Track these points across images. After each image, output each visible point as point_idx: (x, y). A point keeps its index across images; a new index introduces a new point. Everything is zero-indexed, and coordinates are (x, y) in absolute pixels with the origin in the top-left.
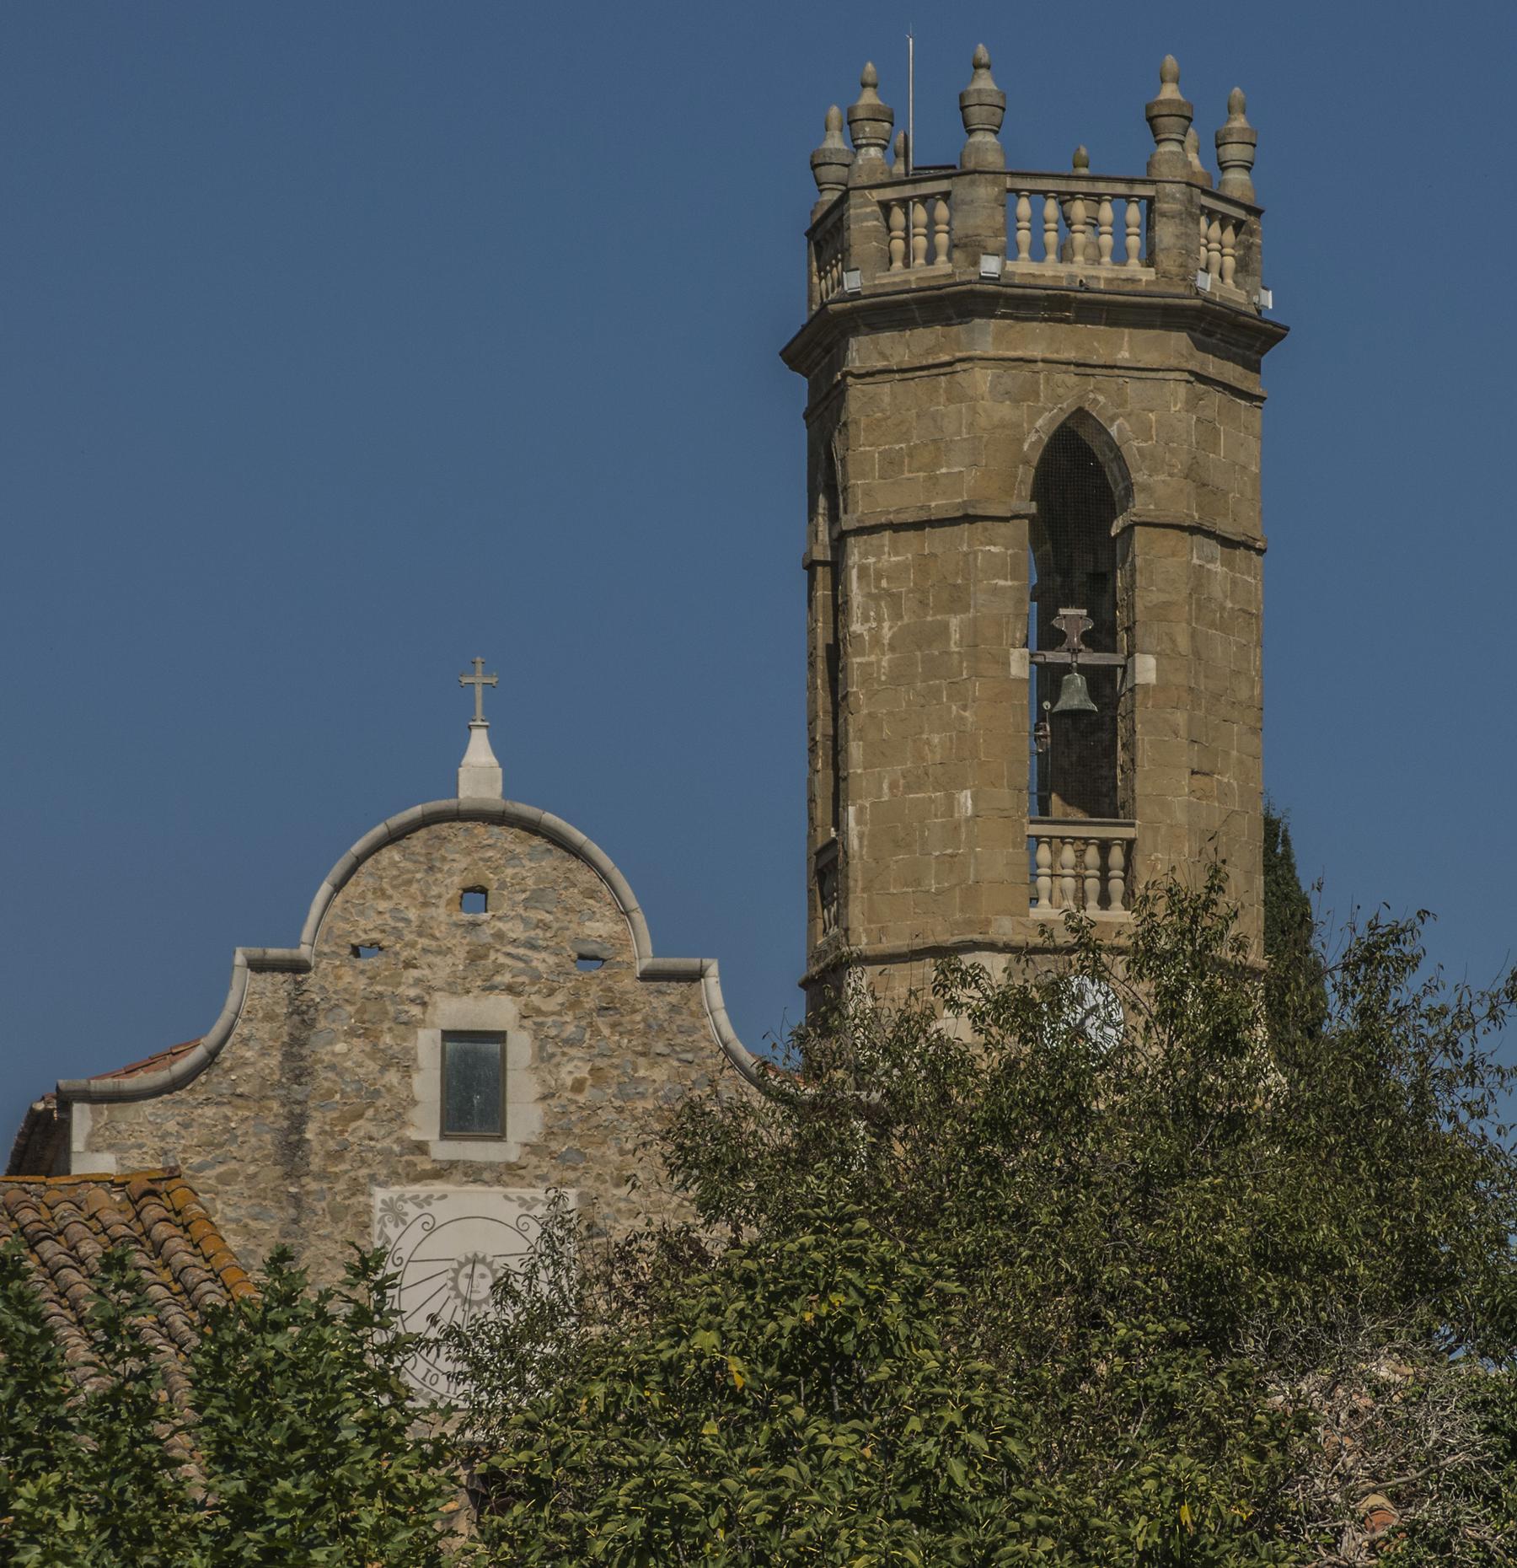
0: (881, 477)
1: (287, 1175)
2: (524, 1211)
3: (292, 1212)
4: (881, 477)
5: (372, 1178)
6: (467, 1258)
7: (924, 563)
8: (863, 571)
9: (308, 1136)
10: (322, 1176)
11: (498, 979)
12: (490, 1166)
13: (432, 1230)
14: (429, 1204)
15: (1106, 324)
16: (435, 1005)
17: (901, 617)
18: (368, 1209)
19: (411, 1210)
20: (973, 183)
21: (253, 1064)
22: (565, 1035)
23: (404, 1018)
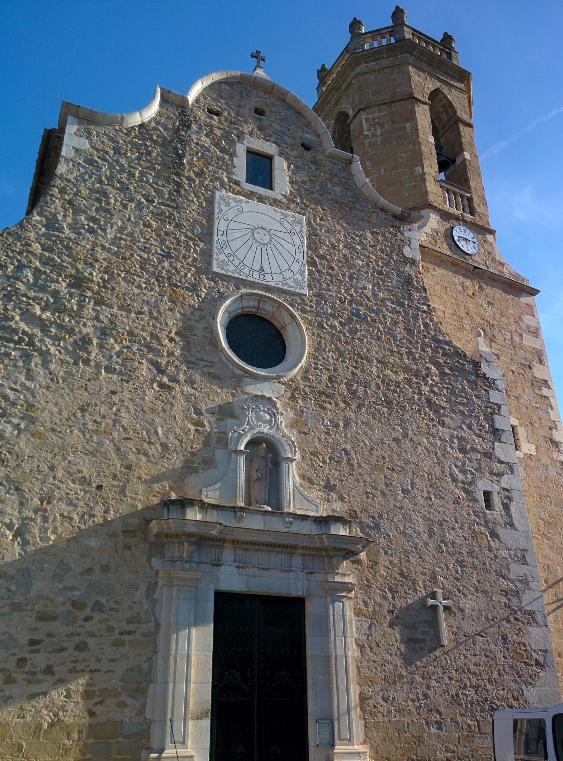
8: (367, 120)
12: (268, 198)
13: (242, 212)
19: (233, 204)
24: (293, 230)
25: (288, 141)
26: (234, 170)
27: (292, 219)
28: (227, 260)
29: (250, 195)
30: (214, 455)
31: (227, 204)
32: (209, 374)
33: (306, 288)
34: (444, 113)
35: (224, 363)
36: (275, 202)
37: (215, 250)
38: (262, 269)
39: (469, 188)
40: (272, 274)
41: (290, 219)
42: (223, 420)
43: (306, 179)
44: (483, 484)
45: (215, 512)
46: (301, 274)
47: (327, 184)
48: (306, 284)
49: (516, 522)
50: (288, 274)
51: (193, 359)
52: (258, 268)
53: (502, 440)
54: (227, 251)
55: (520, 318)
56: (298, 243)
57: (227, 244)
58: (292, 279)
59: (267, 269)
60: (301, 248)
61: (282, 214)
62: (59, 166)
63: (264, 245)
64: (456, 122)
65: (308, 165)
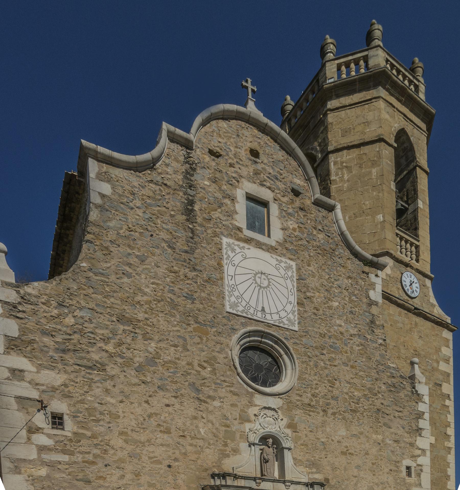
0: (342, 136)
1: (188, 220)
2: (277, 263)
3: (191, 235)
4: (342, 136)
5: (222, 234)
6: (260, 271)
7: (360, 157)
8: (335, 163)
9: (195, 209)
10: (201, 225)
11: (265, 183)
12: (265, 244)
13: (245, 258)
14: (244, 249)
15: (410, 110)
16: (242, 182)
17: (352, 172)
18: (221, 244)
19: (238, 250)
20: (377, 50)
21: (170, 175)
22: (288, 212)
23: (231, 182)
24: (286, 275)
25: (280, 186)
26: (236, 217)
27: (285, 265)
28: (236, 301)
29: (248, 241)
30: (238, 446)
31: (233, 250)
32: (231, 391)
33: (297, 325)
34: (404, 157)
35: (241, 384)
36: (270, 249)
37: (227, 293)
38: (263, 310)
39: (417, 236)
40: (271, 314)
41: (283, 265)
42: (243, 423)
43: (296, 226)
44: (407, 462)
45: (243, 481)
46: (293, 314)
47: (313, 231)
48: (296, 323)
49: (422, 484)
50: (283, 314)
51: (218, 381)
52: (260, 309)
53: (422, 435)
54: (236, 293)
55: (440, 349)
56: (290, 286)
57: (235, 287)
58: (286, 318)
59: (267, 310)
60: (292, 291)
61: (277, 260)
62: (91, 213)
63: (264, 288)
64: (415, 168)
65: (297, 212)
